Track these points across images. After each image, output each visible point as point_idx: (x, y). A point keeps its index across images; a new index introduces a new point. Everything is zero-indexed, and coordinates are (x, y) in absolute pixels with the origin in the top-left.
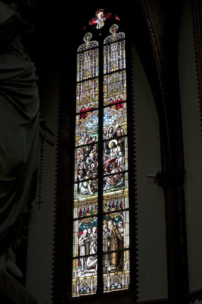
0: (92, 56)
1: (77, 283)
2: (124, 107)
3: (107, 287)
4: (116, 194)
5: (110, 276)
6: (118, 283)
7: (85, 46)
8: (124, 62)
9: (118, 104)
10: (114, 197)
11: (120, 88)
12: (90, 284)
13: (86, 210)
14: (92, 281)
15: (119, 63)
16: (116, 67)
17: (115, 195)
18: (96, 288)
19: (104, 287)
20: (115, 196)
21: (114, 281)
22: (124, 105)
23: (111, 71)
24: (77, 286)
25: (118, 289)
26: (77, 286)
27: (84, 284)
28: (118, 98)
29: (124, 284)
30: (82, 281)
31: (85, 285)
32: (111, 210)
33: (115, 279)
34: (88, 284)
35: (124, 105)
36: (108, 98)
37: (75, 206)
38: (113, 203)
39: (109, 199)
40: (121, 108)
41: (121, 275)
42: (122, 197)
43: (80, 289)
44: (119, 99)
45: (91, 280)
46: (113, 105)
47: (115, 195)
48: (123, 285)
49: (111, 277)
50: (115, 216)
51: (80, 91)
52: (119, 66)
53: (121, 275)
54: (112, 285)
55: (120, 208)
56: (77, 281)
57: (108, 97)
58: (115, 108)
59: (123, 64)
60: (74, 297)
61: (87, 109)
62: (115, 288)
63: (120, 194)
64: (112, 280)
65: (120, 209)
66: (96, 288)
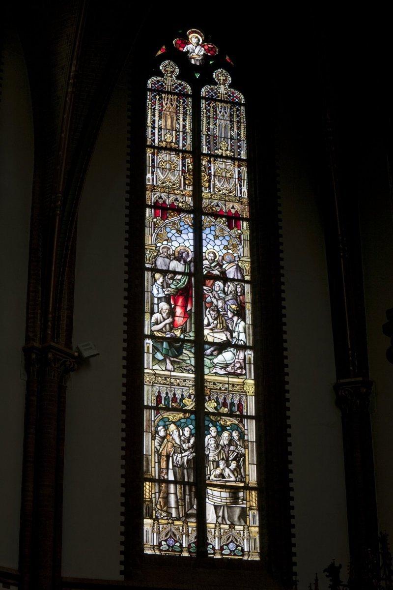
0: (178, 108)
1: (154, 529)
2: (243, 229)
3: (213, 548)
4: (230, 384)
5: (220, 529)
6: (175, 540)
7: (217, 91)
8: (151, 134)
9: (163, 210)
10: (227, 388)
11: (235, 190)
12: (213, 539)
13: (170, 395)
14: (217, 532)
15: (160, 137)
16: (172, 142)
17: (229, 386)
18: (193, 545)
19: (209, 546)
20: (227, 385)
21: (228, 539)
22: (242, 225)
23: (160, 143)
24: (155, 534)
25: (235, 555)
26: (155, 534)
27: (169, 532)
28: (232, 208)
29: (248, 548)
30: (226, 530)
31: (232, 540)
32: (221, 411)
33: (230, 537)
34: (177, 536)
35: (242, 225)
36: (211, 200)
37: (146, 382)
38: (225, 399)
39: (216, 389)
40: (236, 229)
41: (181, 528)
42: (242, 392)
43: (161, 541)
44: (233, 211)
45: (215, 531)
46: (222, 216)
47: (229, 386)
48: (246, 550)
49: (222, 531)
50: (229, 423)
51: (153, 164)
52: (233, 151)
53: (181, 528)
54: (163, 543)
55: (238, 410)
56: (154, 524)
57: (211, 198)
58: (225, 223)
59: (241, 151)
60: (184, 555)
61: (170, 205)
62: (230, 553)
63: (238, 385)
64: (163, 534)
65: (238, 413)
66: (193, 545)
